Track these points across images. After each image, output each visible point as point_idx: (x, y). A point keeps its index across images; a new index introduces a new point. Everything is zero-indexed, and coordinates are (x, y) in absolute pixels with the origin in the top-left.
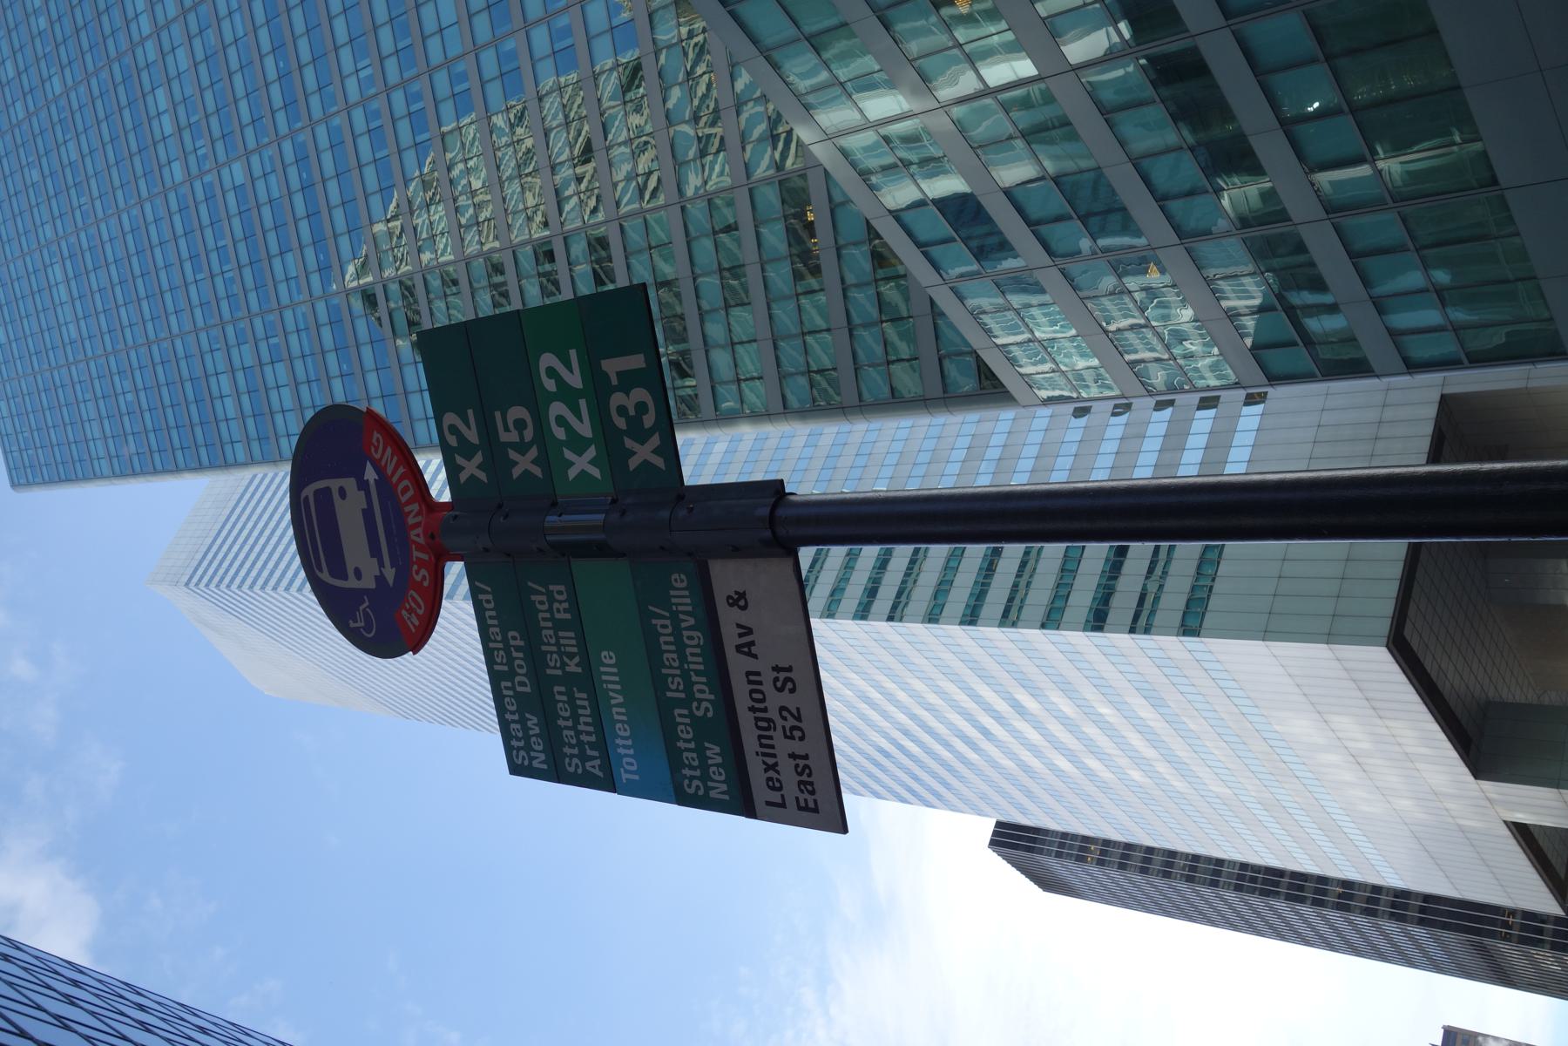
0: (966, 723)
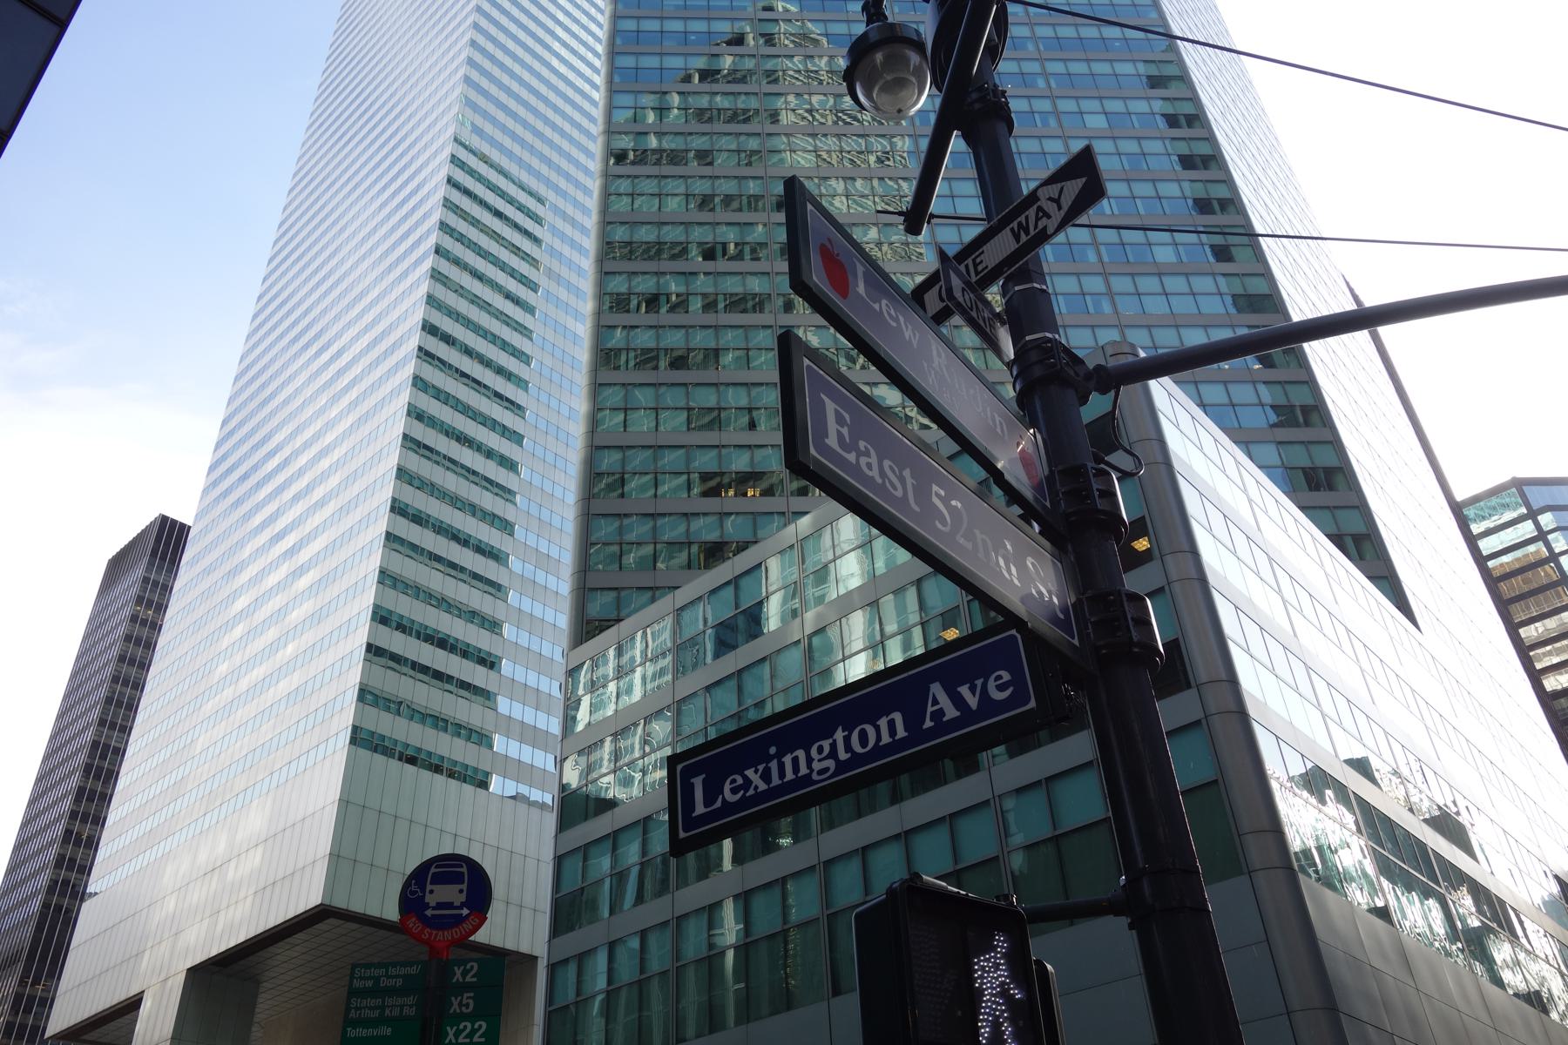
0: (290, 520)
